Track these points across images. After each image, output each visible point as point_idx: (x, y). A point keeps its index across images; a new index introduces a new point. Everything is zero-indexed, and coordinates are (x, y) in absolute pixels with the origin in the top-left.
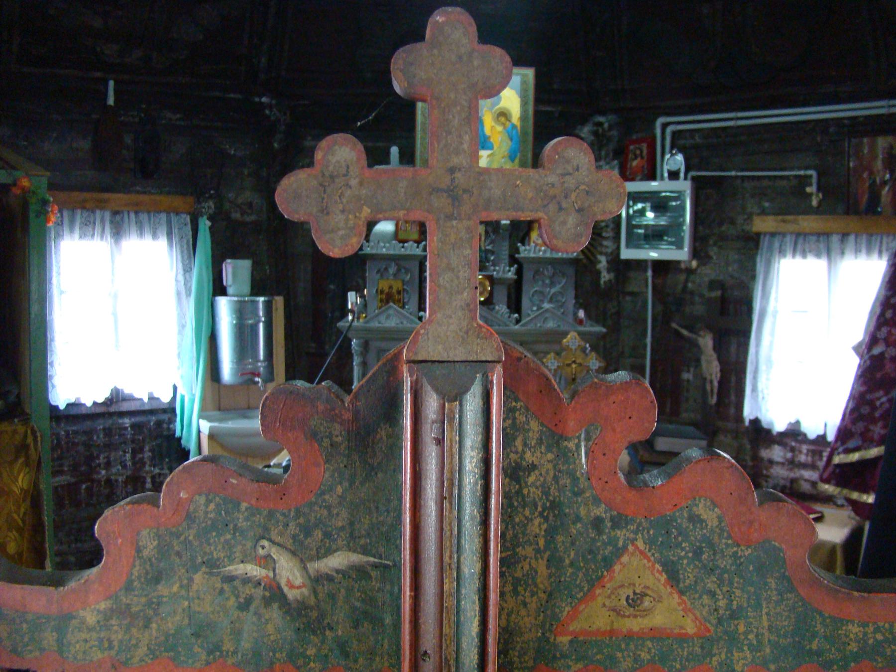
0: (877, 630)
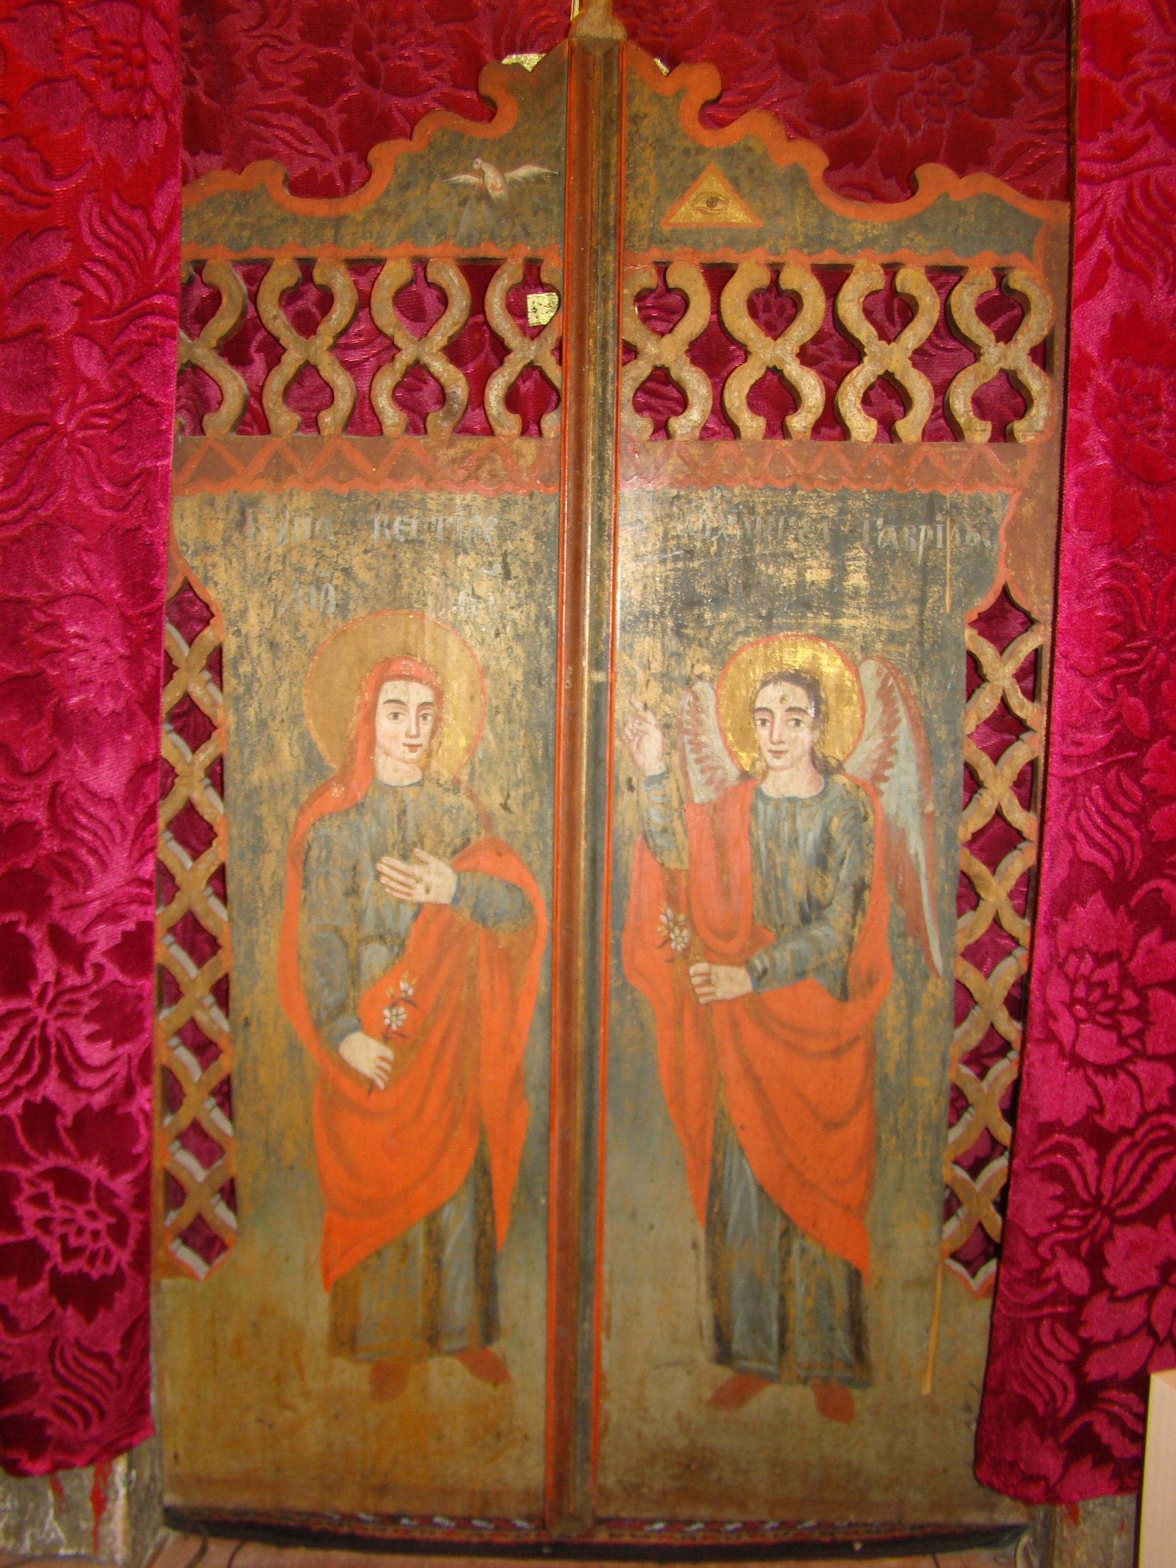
0: (874, 227)
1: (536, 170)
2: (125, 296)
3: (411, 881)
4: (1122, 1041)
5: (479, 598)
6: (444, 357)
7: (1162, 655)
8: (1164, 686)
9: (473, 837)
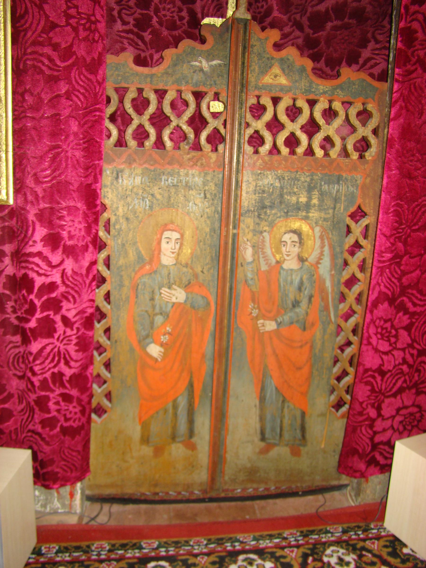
1: (219, 62)
2: (87, 104)
3: (171, 296)
4: (390, 345)
5: (196, 204)
6: (187, 124)
7: (409, 231)
8: (409, 239)
9: (192, 281)
